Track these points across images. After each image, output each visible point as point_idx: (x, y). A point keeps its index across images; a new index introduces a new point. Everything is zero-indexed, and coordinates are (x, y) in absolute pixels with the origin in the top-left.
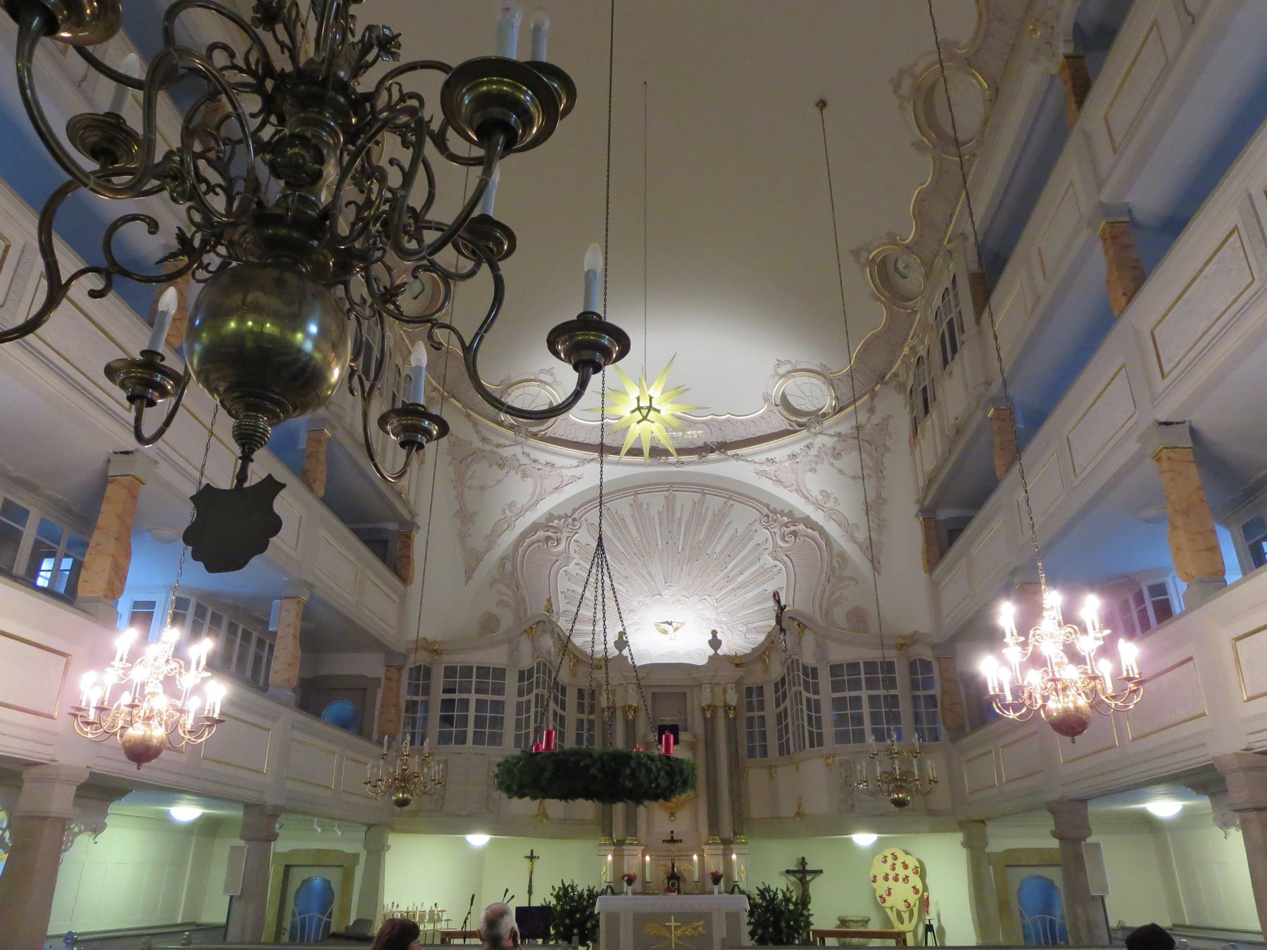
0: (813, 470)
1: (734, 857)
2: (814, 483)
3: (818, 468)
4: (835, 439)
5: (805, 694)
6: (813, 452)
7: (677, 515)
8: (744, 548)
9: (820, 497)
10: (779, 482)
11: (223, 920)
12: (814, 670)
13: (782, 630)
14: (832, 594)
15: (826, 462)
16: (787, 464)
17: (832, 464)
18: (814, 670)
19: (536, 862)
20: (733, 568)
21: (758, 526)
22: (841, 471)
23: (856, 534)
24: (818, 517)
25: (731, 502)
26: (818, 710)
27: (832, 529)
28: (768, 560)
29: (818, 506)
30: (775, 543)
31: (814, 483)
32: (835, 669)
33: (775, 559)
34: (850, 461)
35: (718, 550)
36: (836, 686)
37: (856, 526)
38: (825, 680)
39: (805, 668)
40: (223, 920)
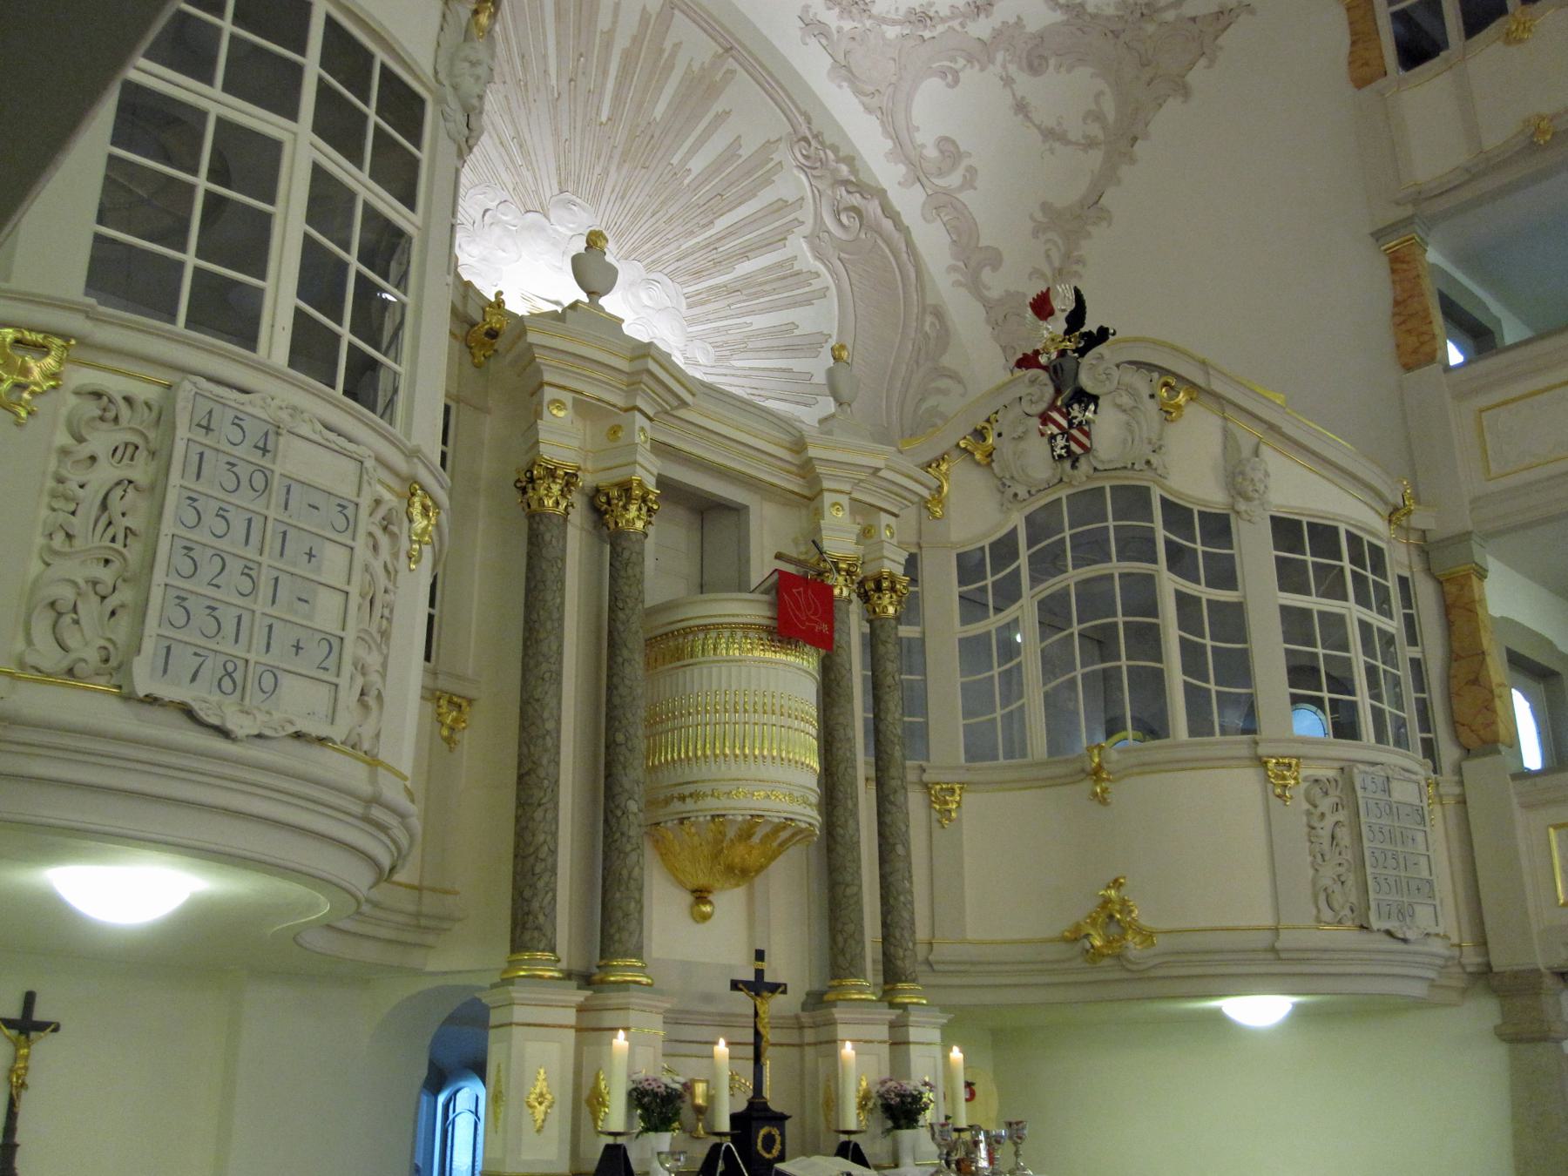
0: (952, 77)
1: (848, 1050)
2: (934, 110)
3: (970, 75)
4: (1059, 16)
5: (1169, 584)
6: (981, 28)
7: (604, 22)
8: (751, 194)
9: (931, 152)
10: (844, 70)
11: (1269, 922)
12: (1218, 527)
13: (48, 565)
14: (922, 400)
15: (995, 69)
16: (892, 32)
17: (1008, 81)
18: (1218, 527)
19: (43, 1045)
20: (731, 232)
21: (782, 154)
22: (1021, 107)
23: (986, 275)
24: (908, 202)
25: (731, 63)
26: (1240, 633)
27: (933, 244)
28: (798, 248)
29: (918, 173)
30: (818, 217)
31: (934, 110)
32: (1286, 530)
33: (819, 256)
34: (1070, 92)
35: (698, 164)
36: (1290, 576)
37: (994, 259)
38: (1255, 552)
39: (1176, 514)
40: (970, 936)
